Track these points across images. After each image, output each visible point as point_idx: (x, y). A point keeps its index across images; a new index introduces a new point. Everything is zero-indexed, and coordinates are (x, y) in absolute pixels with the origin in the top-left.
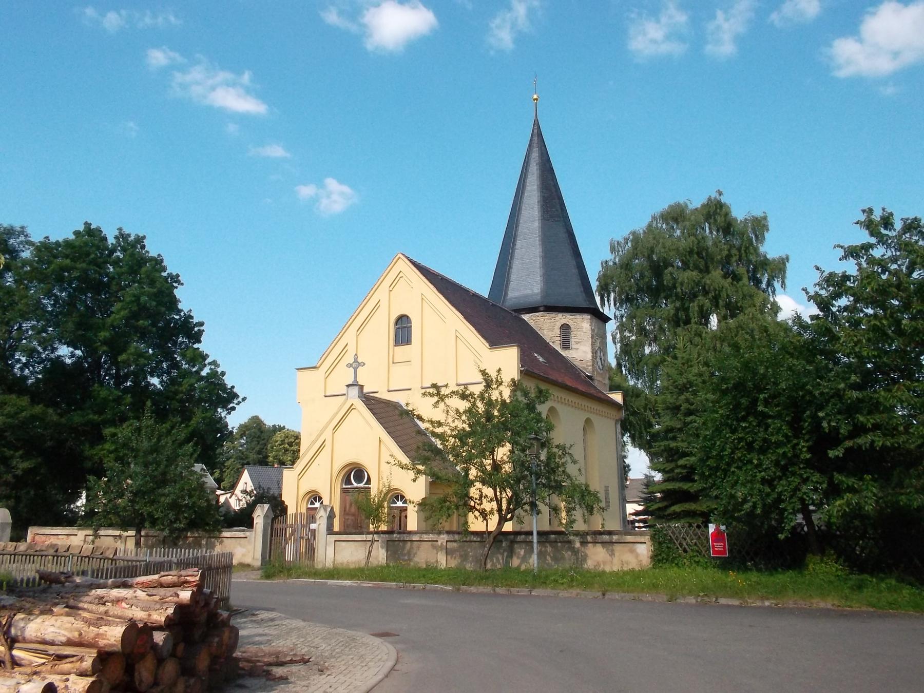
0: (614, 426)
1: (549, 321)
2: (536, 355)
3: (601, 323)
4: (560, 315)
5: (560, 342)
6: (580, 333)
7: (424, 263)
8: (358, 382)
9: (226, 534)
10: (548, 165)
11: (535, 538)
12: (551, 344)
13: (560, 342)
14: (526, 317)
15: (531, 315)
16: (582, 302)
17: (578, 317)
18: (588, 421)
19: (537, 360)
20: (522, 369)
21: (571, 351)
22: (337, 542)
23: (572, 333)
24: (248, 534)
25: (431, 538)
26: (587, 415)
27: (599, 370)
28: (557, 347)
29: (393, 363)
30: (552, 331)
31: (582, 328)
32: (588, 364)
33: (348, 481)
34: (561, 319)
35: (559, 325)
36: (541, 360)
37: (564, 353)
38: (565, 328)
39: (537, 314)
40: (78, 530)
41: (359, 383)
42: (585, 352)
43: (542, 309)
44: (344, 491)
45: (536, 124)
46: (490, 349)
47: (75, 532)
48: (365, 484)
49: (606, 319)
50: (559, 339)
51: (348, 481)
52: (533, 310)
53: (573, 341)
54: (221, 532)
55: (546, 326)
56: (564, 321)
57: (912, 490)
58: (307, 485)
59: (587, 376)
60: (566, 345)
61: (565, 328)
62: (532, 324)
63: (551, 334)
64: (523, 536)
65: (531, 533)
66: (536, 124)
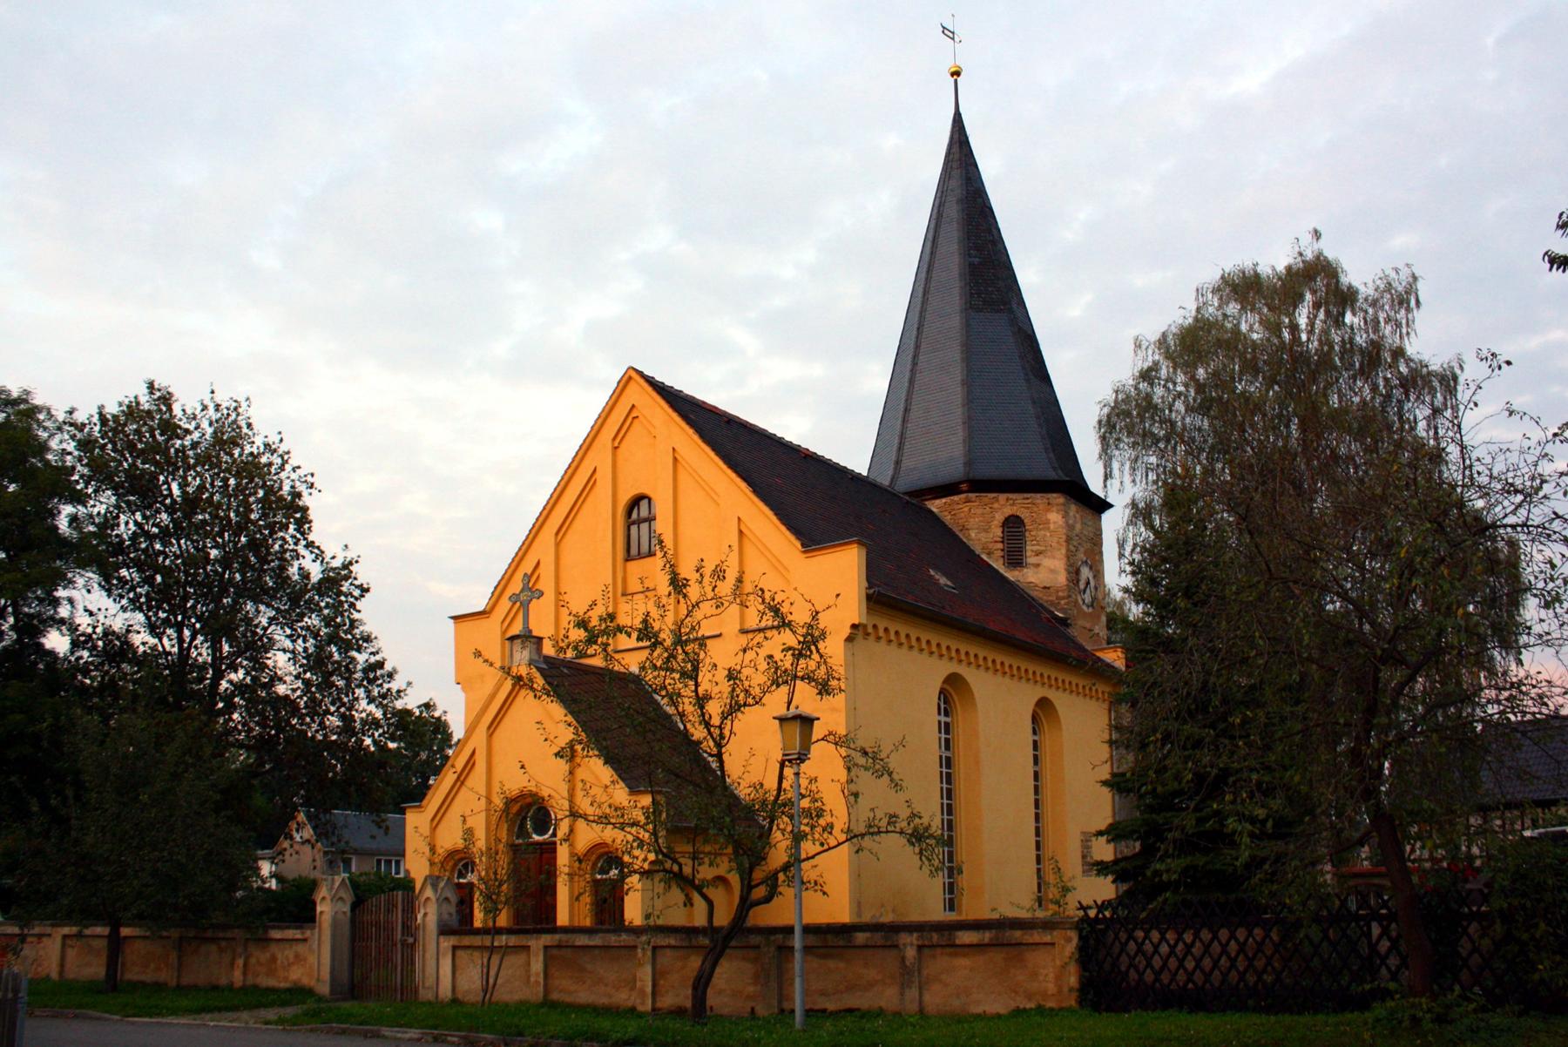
0: (1106, 712)
1: (979, 511)
2: (932, 572)
3: (1089, 515)
4: (1002, 497)
5: (1001, 554)
6: (1042, 532)
7: (659, 377)
8: (530, 631)
9: (276, 934)
10: (980, 200)
11: (797, 941)
12: (984, 557)
13: (1001, 554)
14: (935, 506)
15: (944, 500)
16: (1044, 468)
17: (1039, 499)
18: (1044, 704)
19: (936, 583)
20: (872, 591)
21: (1025, 570)
22: (459, 953)
23: (1027, 534)
24: (308, 933)
25: (624, 940)
26: (1039, 692)
27: (1085, 608)
28: (998, 565)
29: (624, 594)
30: (986, 531)
31: (1048, 522)
32: (1061, 594)
33: (522, 832)
34: (1005, 505)
35: (999, 517)
36: (943, 580)
37: (1011, 575)
38: (1013, 525)
39: (956, 498)
40: (53, 926)
41: (534, 634)
42: (1052, 571)
43: (964, 486)
44: (514, 849)
45: (958, 121)
46: (804, 552)
47: (48, 930)
48: (551, 837)
49: (1102, 506)
50: (1000, 546)
51: (522, 832)
52: (947, 489)
53: (1030, 548)
54: (266, 929)
55: (974, 522)
56: (1008, 511)
57: (1071, 547)
58: (450, 838)
59: (1056, 618)
60: (1015, 558)
61: (1013, 525)
62: (947, 518)
63: (984, 537)
64: (868, 935)
65: (789, 930)
66: (958, 121)
